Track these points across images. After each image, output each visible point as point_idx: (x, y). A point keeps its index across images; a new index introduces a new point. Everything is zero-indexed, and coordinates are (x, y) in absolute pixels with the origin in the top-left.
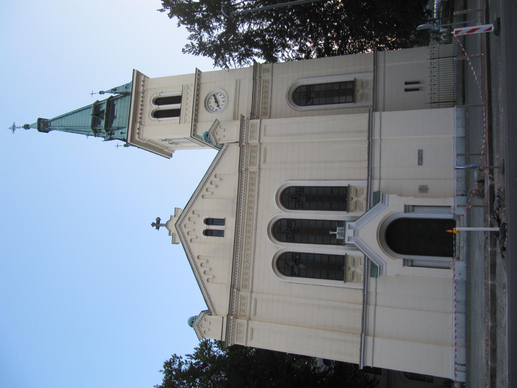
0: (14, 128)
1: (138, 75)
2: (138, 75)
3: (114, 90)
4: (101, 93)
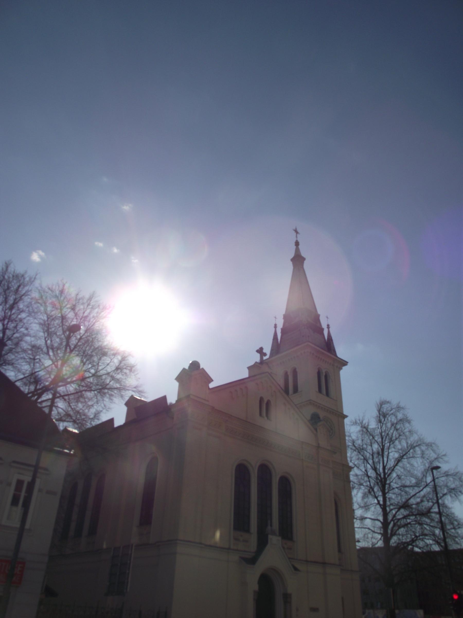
0: (296, 231)
1: (345, 363)
2: (345, 363)
3: (330, 338)
4: (328, 326)
